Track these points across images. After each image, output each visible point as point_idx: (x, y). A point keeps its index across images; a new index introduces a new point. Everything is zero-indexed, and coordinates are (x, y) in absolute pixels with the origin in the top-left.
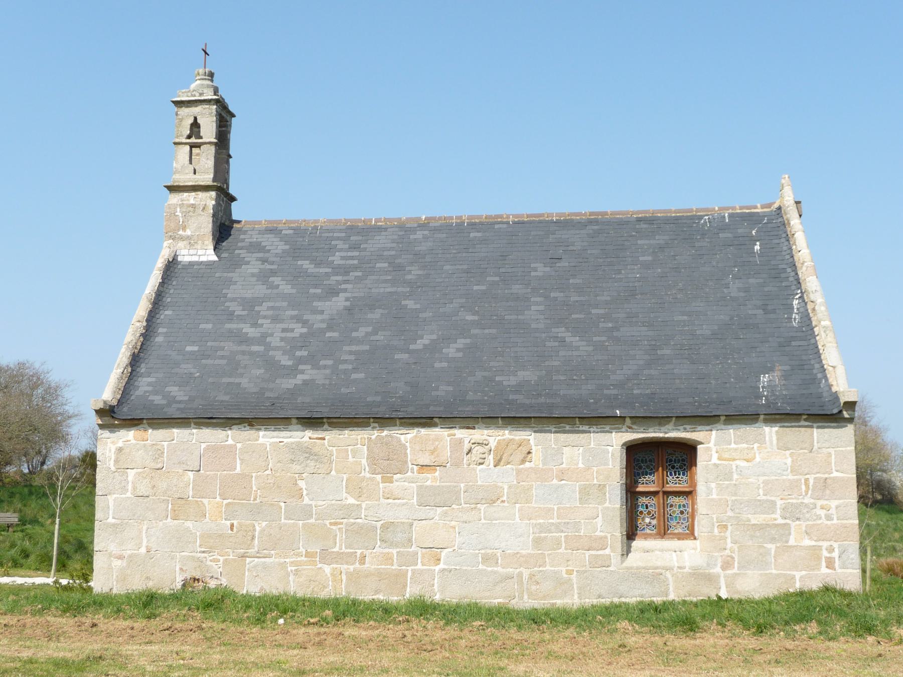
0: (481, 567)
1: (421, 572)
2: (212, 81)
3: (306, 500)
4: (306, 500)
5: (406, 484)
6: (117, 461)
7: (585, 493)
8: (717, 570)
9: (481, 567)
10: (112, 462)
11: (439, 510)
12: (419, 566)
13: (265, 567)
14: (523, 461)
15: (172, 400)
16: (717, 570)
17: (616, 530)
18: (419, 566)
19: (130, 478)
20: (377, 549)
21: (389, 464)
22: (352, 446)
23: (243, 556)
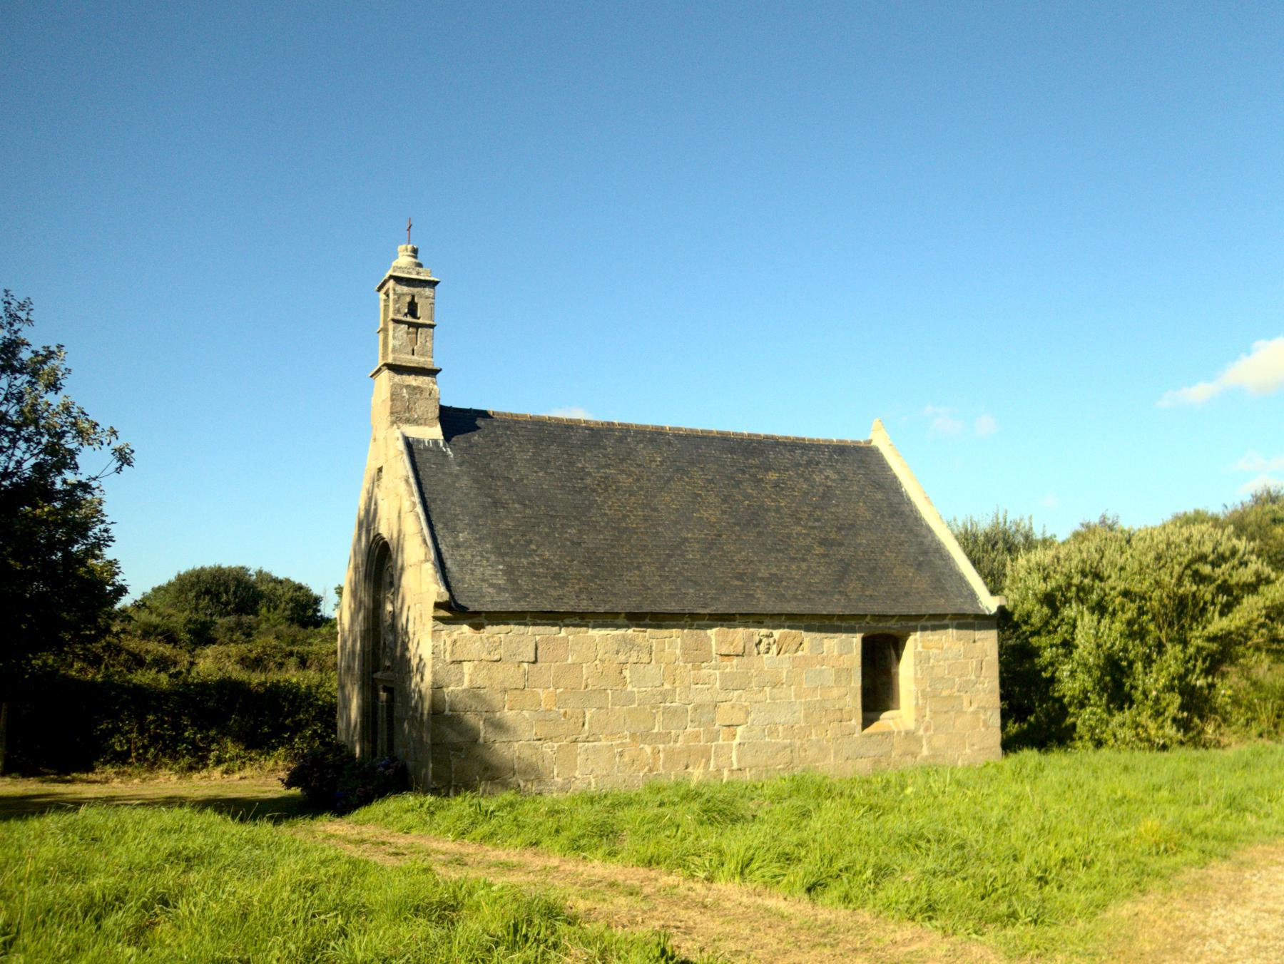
0: (767, 739)
1: (723, 747)
2: (415, 257)
3: (629, 688)
4: (629, 688)
5: (713, 673)
6: (452, 653)
7: (838, 674)
8: (921, 732)
9: (767, 739)
10: (448, 654)
11: (736, 693)
12: (721, 742)
13: (595, 750)
14: (797, 650)
15: (462, 581)
16: (921, 732)
17: (854, 701)
18: (721, 742)
19: (466, 670)
20: (689, 730)
21: (698, 657)
22: (673, 640)
23: (575, 741)
